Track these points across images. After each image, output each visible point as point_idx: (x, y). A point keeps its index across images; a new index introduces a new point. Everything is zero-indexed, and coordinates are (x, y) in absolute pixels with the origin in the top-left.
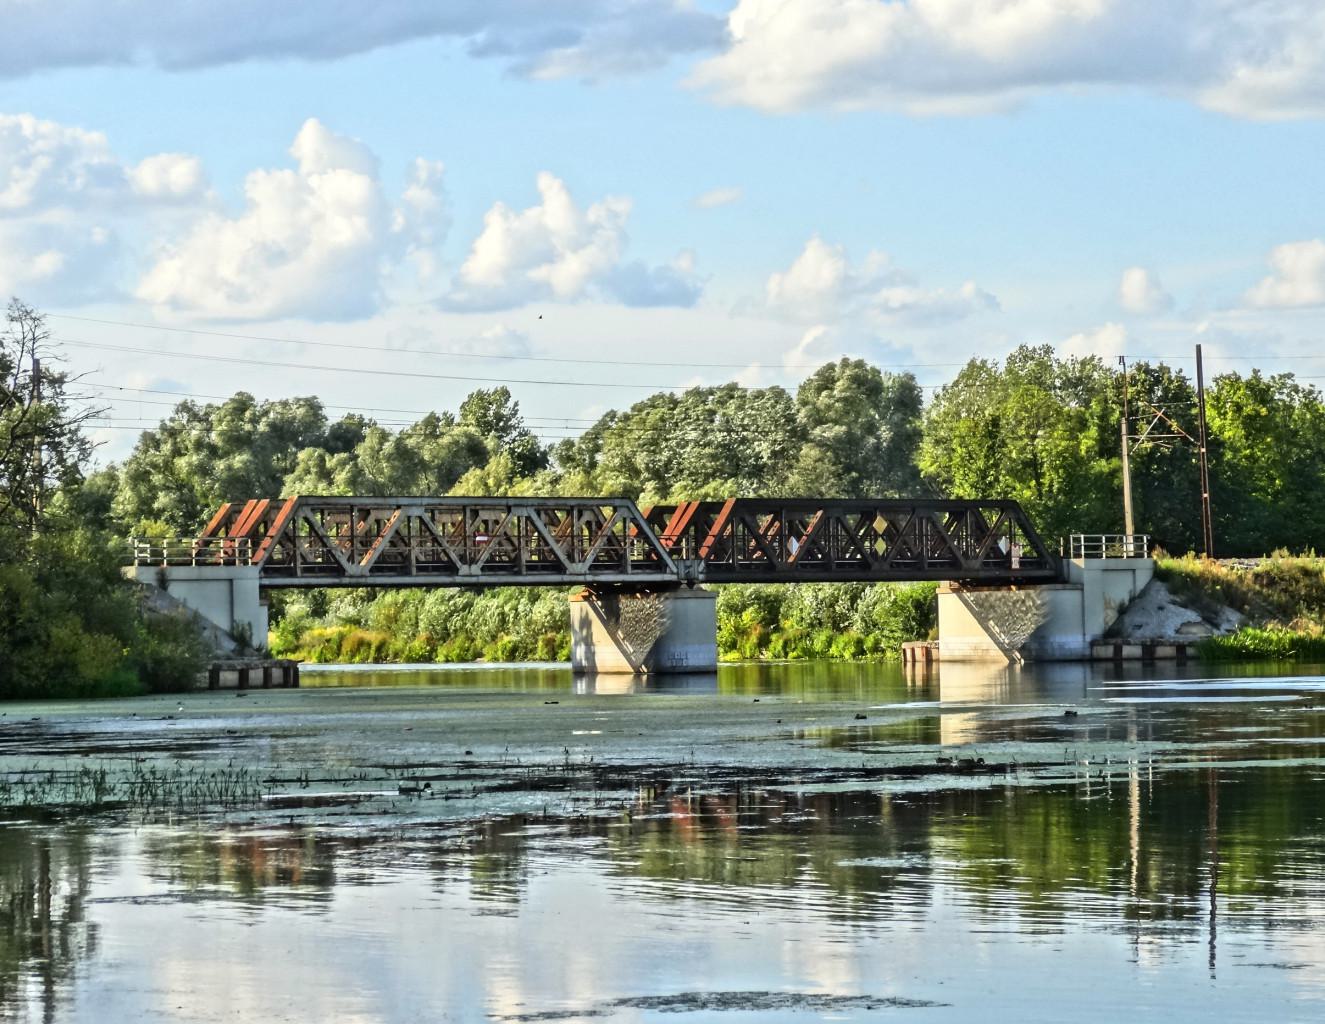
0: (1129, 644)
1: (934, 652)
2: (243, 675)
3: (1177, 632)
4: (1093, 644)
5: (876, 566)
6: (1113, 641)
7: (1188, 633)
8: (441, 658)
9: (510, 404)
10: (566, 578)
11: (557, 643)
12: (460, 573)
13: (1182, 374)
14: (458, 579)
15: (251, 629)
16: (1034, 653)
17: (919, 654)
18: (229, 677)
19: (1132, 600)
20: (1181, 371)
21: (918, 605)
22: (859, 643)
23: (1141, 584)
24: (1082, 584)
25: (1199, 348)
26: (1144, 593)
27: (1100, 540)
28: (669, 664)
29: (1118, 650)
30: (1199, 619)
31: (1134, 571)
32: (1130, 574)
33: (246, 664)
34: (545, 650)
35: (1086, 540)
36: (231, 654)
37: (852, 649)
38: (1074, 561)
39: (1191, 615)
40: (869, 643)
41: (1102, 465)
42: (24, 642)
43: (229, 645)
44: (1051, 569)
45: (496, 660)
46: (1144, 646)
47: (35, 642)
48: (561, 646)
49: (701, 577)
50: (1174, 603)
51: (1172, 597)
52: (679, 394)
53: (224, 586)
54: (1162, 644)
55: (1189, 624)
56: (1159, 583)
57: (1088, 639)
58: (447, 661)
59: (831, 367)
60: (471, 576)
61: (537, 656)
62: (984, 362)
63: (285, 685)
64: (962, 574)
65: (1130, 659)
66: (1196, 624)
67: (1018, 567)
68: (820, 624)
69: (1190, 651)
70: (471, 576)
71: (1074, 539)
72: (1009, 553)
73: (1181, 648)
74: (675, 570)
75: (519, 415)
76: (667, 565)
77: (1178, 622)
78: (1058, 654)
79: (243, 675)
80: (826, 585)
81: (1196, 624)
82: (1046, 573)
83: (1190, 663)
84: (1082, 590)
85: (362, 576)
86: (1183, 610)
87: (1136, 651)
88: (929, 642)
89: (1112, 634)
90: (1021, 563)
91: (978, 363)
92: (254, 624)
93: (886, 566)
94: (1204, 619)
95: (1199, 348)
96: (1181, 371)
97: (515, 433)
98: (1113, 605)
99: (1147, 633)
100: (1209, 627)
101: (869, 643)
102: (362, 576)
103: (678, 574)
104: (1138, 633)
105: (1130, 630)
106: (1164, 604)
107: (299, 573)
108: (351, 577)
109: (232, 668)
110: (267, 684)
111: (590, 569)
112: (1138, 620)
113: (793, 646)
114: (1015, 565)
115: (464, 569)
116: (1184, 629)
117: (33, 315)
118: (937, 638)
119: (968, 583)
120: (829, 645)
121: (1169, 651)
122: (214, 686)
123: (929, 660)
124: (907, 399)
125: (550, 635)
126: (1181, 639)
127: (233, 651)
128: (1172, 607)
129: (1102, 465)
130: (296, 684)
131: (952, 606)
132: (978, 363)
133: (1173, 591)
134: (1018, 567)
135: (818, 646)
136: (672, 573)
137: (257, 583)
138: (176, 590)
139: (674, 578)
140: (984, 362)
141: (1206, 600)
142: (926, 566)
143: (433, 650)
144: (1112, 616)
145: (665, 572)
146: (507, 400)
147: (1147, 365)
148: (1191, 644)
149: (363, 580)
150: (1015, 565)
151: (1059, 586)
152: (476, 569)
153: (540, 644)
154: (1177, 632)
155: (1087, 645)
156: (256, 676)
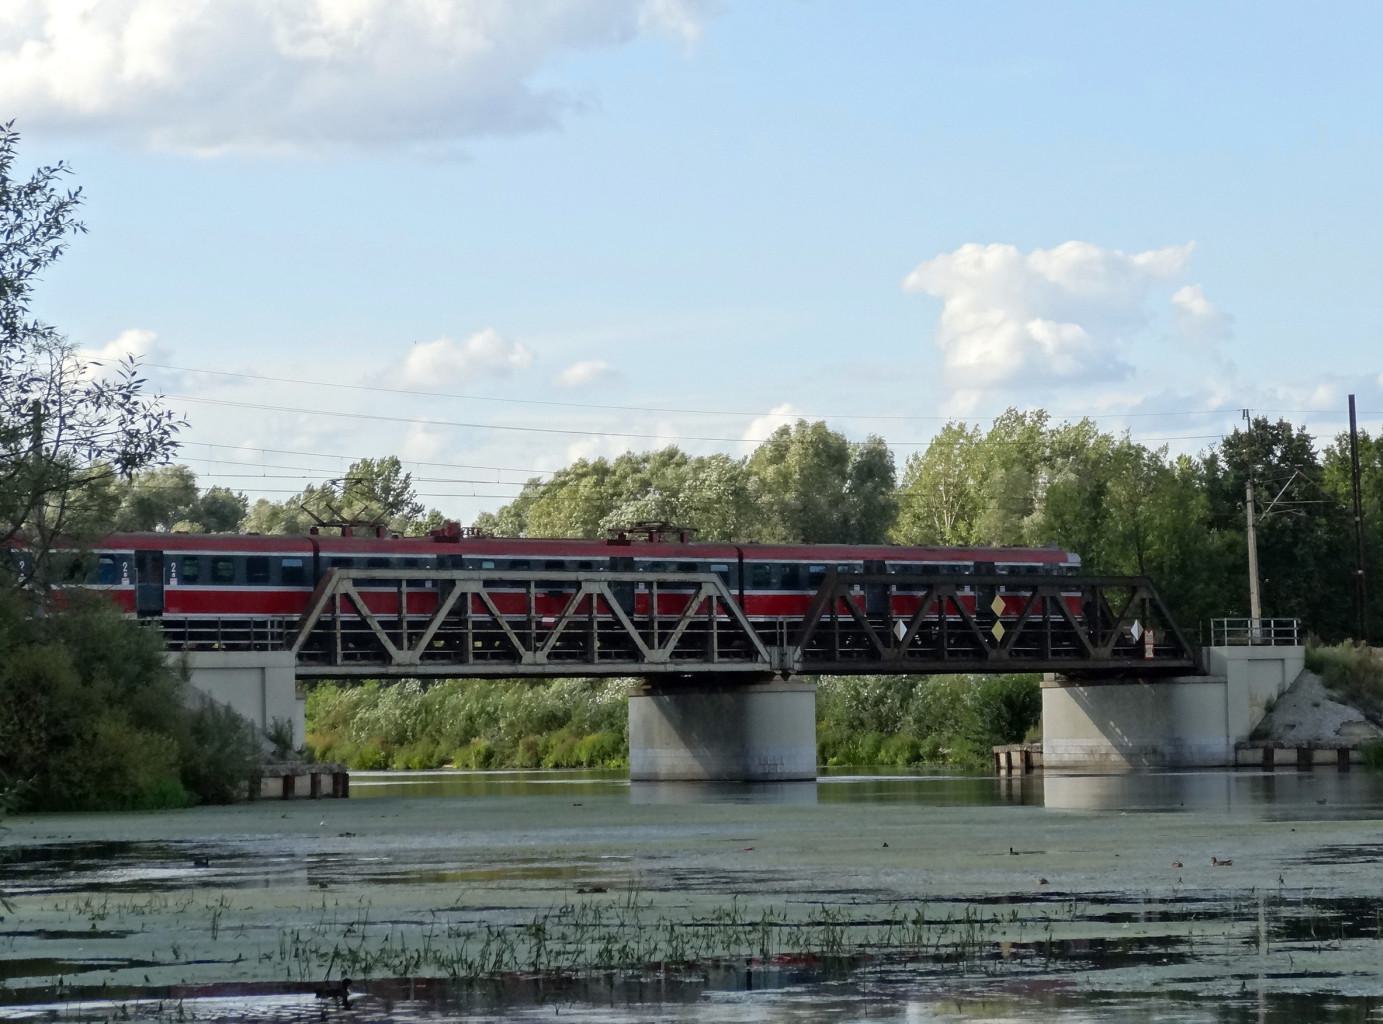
0: (1282, 747)
1: (1035, 757)
2: (288, 782)
3: (1337, 733)
4: (1238, 747)
5: (993, 654)
6: (1262, 743)
7: (1351, 734)
8: (398, 763)
9: (402, 476)
10: (392, 670)
11: (540, 748)
12: (990, 657)
13: (1306, 432)
14: (521, 669)
15: (291, 727)
16: (1168, 758)
17: (1016, 758)
18: (273, 786)
19: (1281, 695)
20: (1304, 428)
21: (1009, 702)
22: (914, 747)
23: (1291, 678)
24: (1226, 676)
25: (1352, 399)
26: (1295, 686)
27: (1292, 622)
28: (760, 770)
29: (1268, 754)
30: (1362, 718)
31: (1283, 660)
32: (1280, 663)
33: (292, 770)
34: (528, 755)
35: (1277, 624)
36: (272, 758)
37: (907, 755)
38: (1214, 649)
39: (1353, 713)
40: (925, 749)
41: (1215, 539)
42: (61, 742)
43: (269, 747)
44: (1189, 659)
45: (467, 766)
46: (1299, 749)
47: (78, 742)
48: (546, 751)
49: (797, 667)
50: (1331, 699)
51: (1329, 692)
52: (611, 463)
53: (255, 677)
54: (1322, 748)
55: (1349, 723)
56: (1312, 676)
57: (1233, 742)
58: (408, 768)
59: (785, 431)
60: (536, 664)
61: (517, 762)
62: (962, 426)
63: (334, 795)
64: (644, 668)
65: (1284, 765)
66: (1358, 723)
67: (1152, 656)
68: (862, 724)
69: (1354, 755)
70: (536, 664)
71: (1216, 623)
72: (1142, 637)
73: (1343, 752)
74: (767, 658)
75: (411, 489)
76: (758, 652)
77: (1337, 721)
78: (1197, 761)
79: (288, 782)
80: (871, 679)
81: (1358, 723)
82: (1184, 663)
83: (1353, 769)
84: (1226, 683)
85: (411, 665)
86: (1341, 706)
87: (1291, 756)
88: (1026, 746)
89: (1257, 736)
90: (1156, 652)
91: (955, 427)
92: (292, 720)
93: (1004, 654)
94: (1368, 717)
95: (1352, 399)
96: (1304, 428)
97: (407, 510)
98: (1259, 700)
99: (1303, 734)
100: (1373, 727)
101: (925, 749)
102: (411, 665)
103: (771, 663)
104: (1291, 734)
105: (1280, 730)
106: (1320, 700)
107: (339, 660)
108: (399, 665)
109: (275, 775)
110: (314, 794)
111: (421, 658)
112: (1289, 718)
113: (832, 751)
114: (1149, 654)
115: (527, 656)
116: (1346, 730)
117: (62, 344)
118: (1040, 740)
119: (1071, 678)
120: (878, 750)
121: (1330, 756)
122: (254, 797)
123: (1029, 766)
124: (876, 466)
125: (531, 738)
126: (1344, 741)
127: (274, 753)
128: (1330, 704)
129: (1215, 539)
130: (345, 795)
131: (1057, 702)
132: (955, 427)
133: (1329, 685)
134: (1152, 656)
135: (862, 752)
136: (765, 662)
137: (291, 674)
138: (198, 681)
139: (766, 668)
140: (962, 426)
141: (1368, 696)
142: (838, 655)
143: (389, 756)
144: (1259, 713)
145: (390, 664)
146: (397, 472)
147: (1265, 420)
148: (1355, 748)
149: (412, 670)
150: (1149, 654)
151: (1198, 678)
152: (541, 656)
153: (521, 748)
154: (1337, 733)
155: (1232, 749)
156: (303, 785)
